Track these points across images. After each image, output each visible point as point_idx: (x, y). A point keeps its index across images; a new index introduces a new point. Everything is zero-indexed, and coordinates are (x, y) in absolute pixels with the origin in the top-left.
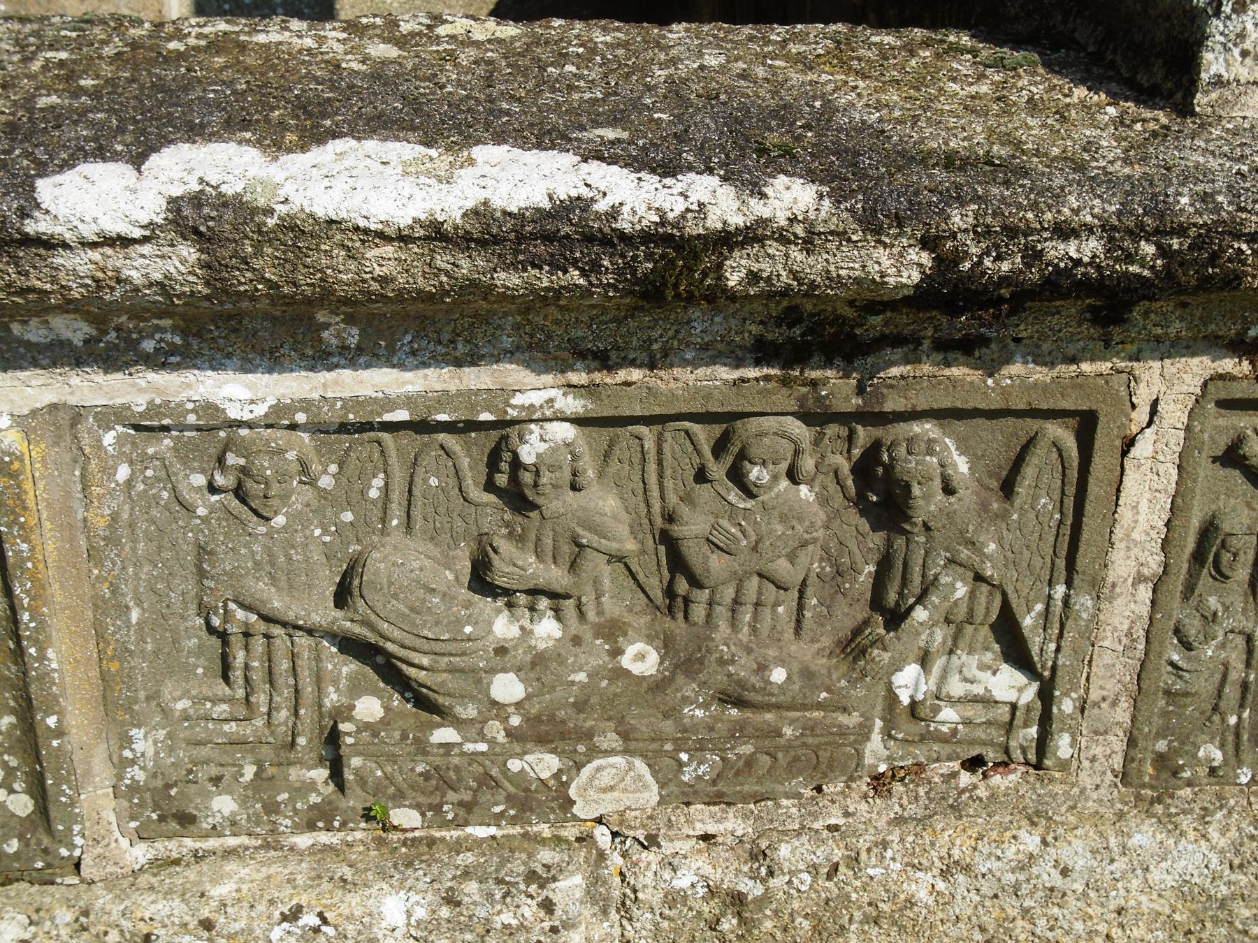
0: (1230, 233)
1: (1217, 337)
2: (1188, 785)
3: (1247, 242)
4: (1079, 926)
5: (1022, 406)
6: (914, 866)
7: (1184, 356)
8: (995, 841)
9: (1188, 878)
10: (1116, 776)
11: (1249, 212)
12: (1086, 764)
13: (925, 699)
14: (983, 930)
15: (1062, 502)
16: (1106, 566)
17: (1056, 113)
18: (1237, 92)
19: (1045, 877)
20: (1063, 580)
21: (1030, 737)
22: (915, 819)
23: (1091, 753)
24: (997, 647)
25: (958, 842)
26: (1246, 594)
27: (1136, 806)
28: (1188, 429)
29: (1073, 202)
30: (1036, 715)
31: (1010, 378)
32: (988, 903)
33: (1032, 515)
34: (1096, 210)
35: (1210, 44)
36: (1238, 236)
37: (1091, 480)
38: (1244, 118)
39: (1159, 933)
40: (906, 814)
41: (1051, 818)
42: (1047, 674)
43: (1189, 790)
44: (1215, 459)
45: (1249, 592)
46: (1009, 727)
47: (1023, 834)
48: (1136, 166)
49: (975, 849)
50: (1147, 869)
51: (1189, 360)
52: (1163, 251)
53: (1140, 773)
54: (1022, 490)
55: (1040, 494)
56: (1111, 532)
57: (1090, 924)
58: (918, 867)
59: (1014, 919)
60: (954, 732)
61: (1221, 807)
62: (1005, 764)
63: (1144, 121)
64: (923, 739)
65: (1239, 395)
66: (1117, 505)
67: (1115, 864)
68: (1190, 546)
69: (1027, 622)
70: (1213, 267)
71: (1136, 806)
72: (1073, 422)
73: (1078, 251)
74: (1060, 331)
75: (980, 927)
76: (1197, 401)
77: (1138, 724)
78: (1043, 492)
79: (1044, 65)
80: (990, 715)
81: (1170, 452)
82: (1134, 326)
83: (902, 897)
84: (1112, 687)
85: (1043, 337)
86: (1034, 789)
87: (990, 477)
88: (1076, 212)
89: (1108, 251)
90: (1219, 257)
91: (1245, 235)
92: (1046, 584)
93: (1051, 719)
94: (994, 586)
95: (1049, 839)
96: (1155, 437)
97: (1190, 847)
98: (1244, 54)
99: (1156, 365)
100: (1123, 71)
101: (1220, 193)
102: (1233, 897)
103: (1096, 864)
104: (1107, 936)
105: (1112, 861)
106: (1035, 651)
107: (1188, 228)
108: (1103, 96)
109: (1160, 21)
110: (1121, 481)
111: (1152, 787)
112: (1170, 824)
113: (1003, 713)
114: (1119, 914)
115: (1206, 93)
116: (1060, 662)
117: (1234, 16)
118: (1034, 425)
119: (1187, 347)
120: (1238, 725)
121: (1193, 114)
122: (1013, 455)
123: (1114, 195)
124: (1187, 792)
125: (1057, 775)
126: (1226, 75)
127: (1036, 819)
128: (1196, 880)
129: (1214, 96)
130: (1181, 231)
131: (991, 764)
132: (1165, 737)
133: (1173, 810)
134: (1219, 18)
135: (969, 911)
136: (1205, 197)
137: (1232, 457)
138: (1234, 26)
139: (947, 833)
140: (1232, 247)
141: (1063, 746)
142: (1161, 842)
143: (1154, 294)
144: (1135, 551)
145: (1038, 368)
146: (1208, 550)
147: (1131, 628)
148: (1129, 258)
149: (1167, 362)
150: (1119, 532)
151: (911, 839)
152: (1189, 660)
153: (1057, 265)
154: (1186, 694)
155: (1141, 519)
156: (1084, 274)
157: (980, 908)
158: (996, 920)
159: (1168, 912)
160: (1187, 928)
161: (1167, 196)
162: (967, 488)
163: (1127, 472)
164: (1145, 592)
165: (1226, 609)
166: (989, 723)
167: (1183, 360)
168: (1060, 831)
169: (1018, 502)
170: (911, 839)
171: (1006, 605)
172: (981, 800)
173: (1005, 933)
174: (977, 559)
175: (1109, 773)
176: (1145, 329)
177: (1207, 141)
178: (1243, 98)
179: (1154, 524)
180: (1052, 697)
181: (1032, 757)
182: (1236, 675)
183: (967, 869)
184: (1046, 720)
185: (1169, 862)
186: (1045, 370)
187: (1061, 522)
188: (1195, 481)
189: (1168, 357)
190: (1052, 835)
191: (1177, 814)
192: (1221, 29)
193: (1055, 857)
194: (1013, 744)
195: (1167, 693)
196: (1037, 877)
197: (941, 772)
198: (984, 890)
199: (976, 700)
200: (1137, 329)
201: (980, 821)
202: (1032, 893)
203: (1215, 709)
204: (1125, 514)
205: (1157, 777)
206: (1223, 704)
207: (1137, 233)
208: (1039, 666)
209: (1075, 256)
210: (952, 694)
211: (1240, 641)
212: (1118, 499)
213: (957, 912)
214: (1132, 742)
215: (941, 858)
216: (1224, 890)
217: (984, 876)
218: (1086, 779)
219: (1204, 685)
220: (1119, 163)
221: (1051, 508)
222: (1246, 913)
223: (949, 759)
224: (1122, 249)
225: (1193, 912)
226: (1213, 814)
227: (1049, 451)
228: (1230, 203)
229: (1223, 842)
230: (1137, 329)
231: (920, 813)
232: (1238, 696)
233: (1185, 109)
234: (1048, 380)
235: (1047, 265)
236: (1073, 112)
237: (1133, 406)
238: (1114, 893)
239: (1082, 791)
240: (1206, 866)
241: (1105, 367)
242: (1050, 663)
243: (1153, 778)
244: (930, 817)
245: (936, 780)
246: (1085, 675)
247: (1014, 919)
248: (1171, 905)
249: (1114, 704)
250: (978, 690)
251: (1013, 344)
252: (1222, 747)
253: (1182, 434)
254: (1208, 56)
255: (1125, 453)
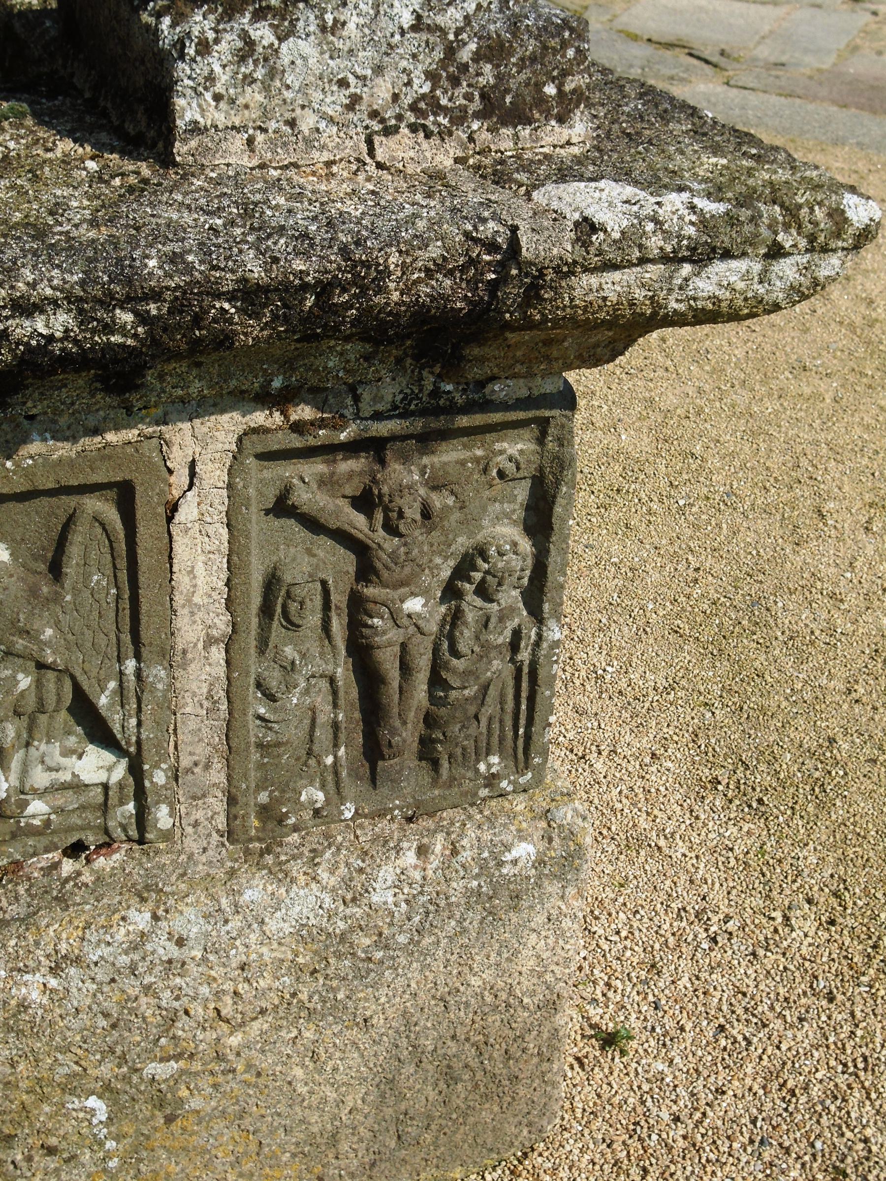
0: (208, 294)
1: (242, 392)
2: (295, 831)
3: (229, 301)
4: (205, 990)
5: (50, 485)
6: (19, 970)
7: (213, 414)
8: (103, 927)
9: (304, 921)
10: (222, 836)
11: (223, 270)
12: (189, 830)
13: (8, 796)
14: (106, 1015)
15: (115, 576)
16: (172, 634)
17: (29, 171)
18: (216, 138)
19: (161, 951)
20: (131, 654)
21: (128, 814)
22: (18, 919)
23: (191, 819)
24: (79, 730)
25: (64, 936)
26: (321, 638)
27: (246, 861)
28: (230, 486)
29: (28, 275)
30: (130, 790)
31: (31, 457)
32: (106, 989)
33: (87, 594)
34: (55, 282)
35: (180, 88)
36: (218, 296)
37: (139, 551)
38: (228, 165)
39: (286, 978)
40: (7, 916)
41: (161, 890)
42: (132, 749)
43: (296, 835)
44: (267, 512)
45: (323, 636)
46: (105, 808)
47: (132, 914)
48: (103, 228)
49: (83, 939)
50: (263, 922)
51: (219, 417)
52: (142, 318)
53: (245, 829)
54: (71, 569)
55: (91, 572)
56: (171, 600)
57: (215, 985)
58: (25, 970)
59: (136, 999)
60: (47, 823)
61: (329, 846)
62: (108, 845)
63: (123, 175)
64: (14, 836)
65: (276, 447)
66: (171, 572)
67: (230, 924)
68: (256, 600)
69: (103, 701)
70: (200, 329)
71: (246, 861)
72: (112, 494)
73: (47, 326)
74: (73, 404)
75: (103, 1013)
76: (234, 457)
77: (235, 782)
78: (94, 569)
79: (35, 115)
80: (82, 799)
81: (216, 512)
82: (152, 390)
83: (13, 1002)
84: (202, 751)
85: (57, 412)
86: (141, 864)
87: (36, 560)
88: (33, 285)
89: (82, 323)
90: (202, 319)
91: (223, 293)
92: (115, 661)
93: (144, 793)
94: (60, 671)
95: (160, 912)
96: (197, 499)
97: (302, 892)
98: (217, 98)
99: (186, 426)
100: (114, 119)
101: (190, 251)
102: (352, 930)
103: (210, 928)
104: (235, 993)
105: (226, 921)
106: (116, 728)
107: (161, 293)
108: (88, 149)
109: (137, 64)
110: (171, 549)
111: (260, 840)
112: (281, 874)
113: (97, 795)
114: (243, 969)
115: (185, 141)
116: (143, 736)
117: (198, 59)
118: (70, 502)
119: (215, 405)
120: (335, 763)
121: (175, 164)
122: (55, 535)
123: (75, 263)
124: (295, 838)
125: (162, 846)
126: (201, 120)
127: (146, 895)
128: (313, 921)
129: (193, 144)
130: (156, 295)
131: (92, 848)
132: (265, 789)
133: (283, 858)
134: (184, 61)
135: (88, 1001)
136: (174, 258)
137: (282, 507)
138: (201, 68)
139: (52, 929)
140: (214, 307)
141: (162, 817)
142: (273, 894)
143: (146, 362)
144: (199, 616)
145: (60, 444)
146: (275, 601)
147: (210, 690)
148: (108, 328)
149: (197, 422)
150: (179, 600)
151: (13, 942)
152: (275, 711)
153: (28, 344)
154: (278, 744)
155: (199, 583)
156: (63, 350)
157: (99, 995)
158: (118, 1003)
159: (290, 957)
160: (312, 968)
161: (134, 260)
162: (11, 576)
163: (175, 538)
164: (218, 654)
165: (303, 656)
166: (82, 808)
167: (213, 418)
168: (171, 902)
169: (68, 584)
170: (13, 942)
171: (77, 688)
172: (87, 885)
173: (130, 1014)
174: (35, 648)
175: (214, 834)
176: (164, 392)
177: (186, 194)
178: (224, 145)
179: (214, 585)
180: (142, 771)
181: (133, 833)
182: (323, 718)
183: (77, 961)
184: (140, 794)
185: (284, 911)
186: (67, 445)
187: (118, 597)
188: (247, 537)
189: (197, 417)
190: (162, 908)
191: (288, 861)
192: (188, 72)
193: (167, 930)
194: (111, 824)
195: (260, 746)
196: (153, 953)
197: (39, 866)
198: (99, 977)
199: (65, 787)
200: (155, 393)
201: (88, 907)
202: (150, 970)
203: (310, 753)
204: (182, 580)
205: (263, 829)
206: (316, 748)
207: (108, 301)
208: (123, 743)
209: (44, 332)
210: (36, 786)
211: (324, 684)
212: (171, 566)
213: (75, 1004)
214: (232, 801)
215: (48, 956)
216: (341, 925)
217: (96, 964)
218: (192, 845)
219: (294, 733)
220: (85, 226)
221: (105, 583)
222: (367, 941)
223: (47, 850)
224: (96, 320)
225: (316, 953)
226: (323, 852)
227: (92, 527)
228: (201, 262)
229: (333, 881)
230: (155, 393)
231: (23, 911)
232: (331, 736)
233: (166, 160)
234: (73, 455)
235: (17, 345)
236: (47, 169)
237: (170, 472)
238: (234, 951)
239: (190, 857)
240: (320, 907)
241: (132, 434)
242: (134, 739)
243: (260, 831)
244: (35, 914)
245: (36, 875)
246: (172, 744)
247: (136, 999)
248: (293, 950)
249: (207, 767)
250: (65, 777)
251: (26, 422)
252: (323, 787)
253: (225, 493)
254: (180, 102)
255: (170, 519)
